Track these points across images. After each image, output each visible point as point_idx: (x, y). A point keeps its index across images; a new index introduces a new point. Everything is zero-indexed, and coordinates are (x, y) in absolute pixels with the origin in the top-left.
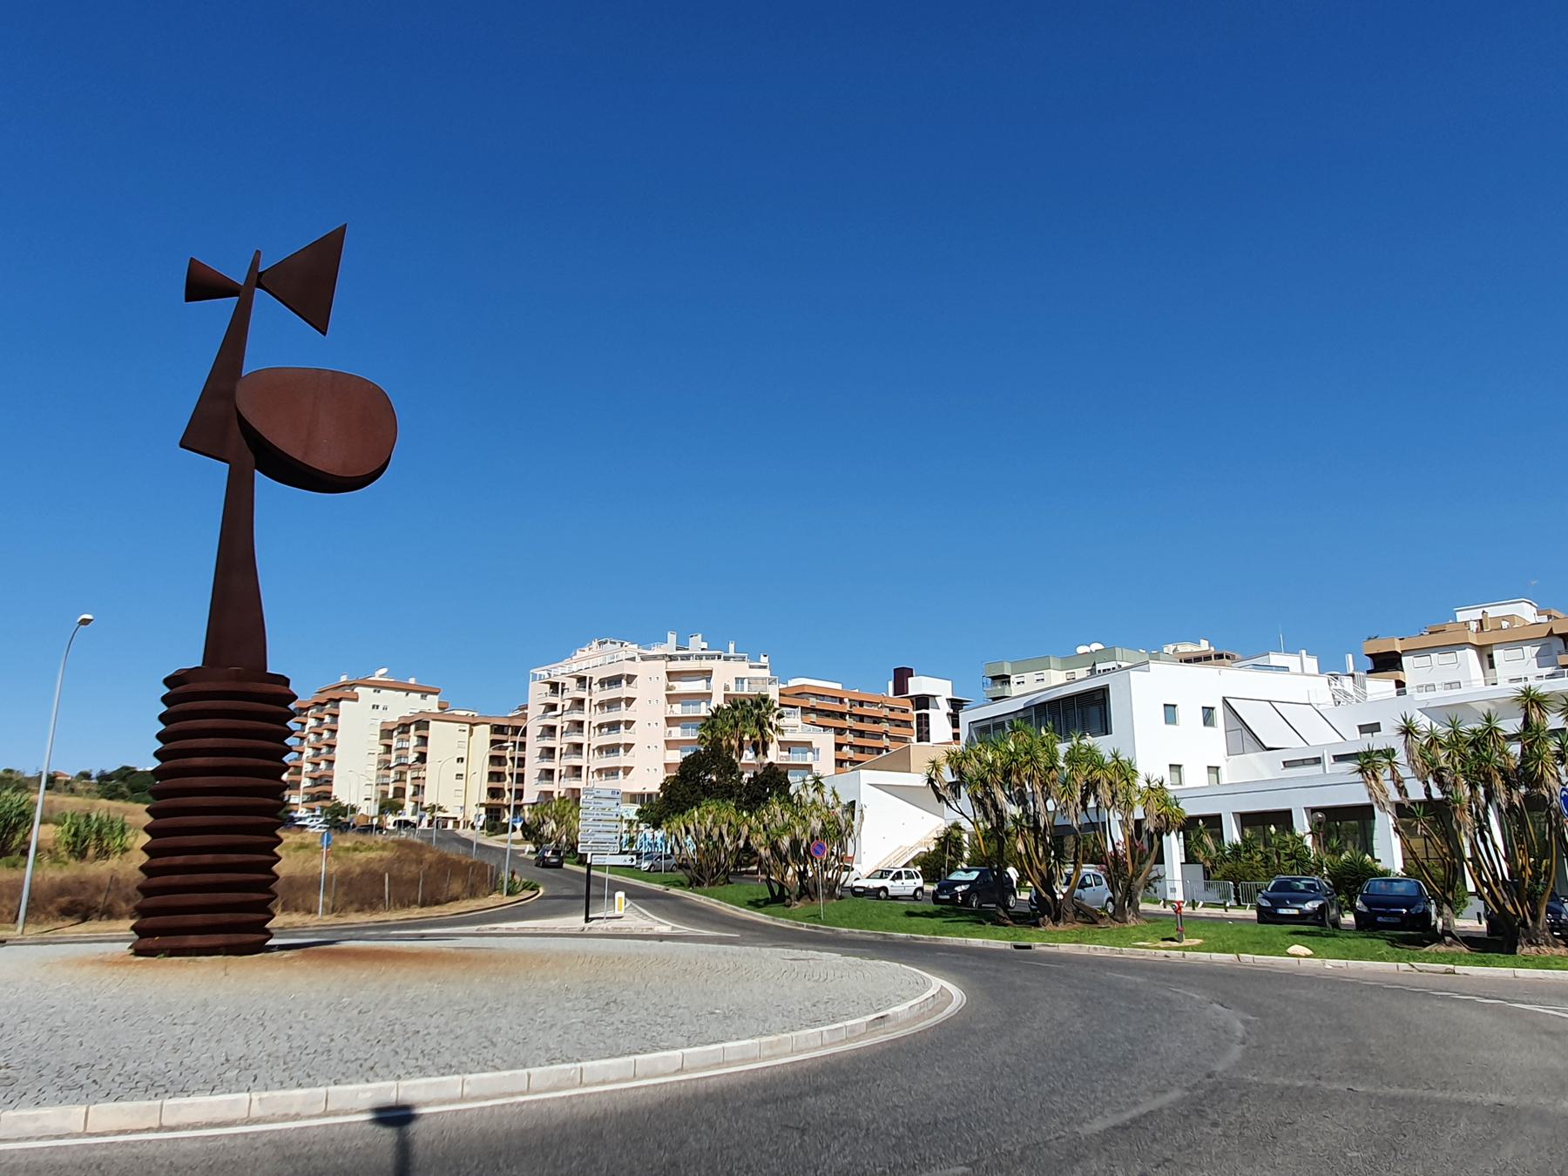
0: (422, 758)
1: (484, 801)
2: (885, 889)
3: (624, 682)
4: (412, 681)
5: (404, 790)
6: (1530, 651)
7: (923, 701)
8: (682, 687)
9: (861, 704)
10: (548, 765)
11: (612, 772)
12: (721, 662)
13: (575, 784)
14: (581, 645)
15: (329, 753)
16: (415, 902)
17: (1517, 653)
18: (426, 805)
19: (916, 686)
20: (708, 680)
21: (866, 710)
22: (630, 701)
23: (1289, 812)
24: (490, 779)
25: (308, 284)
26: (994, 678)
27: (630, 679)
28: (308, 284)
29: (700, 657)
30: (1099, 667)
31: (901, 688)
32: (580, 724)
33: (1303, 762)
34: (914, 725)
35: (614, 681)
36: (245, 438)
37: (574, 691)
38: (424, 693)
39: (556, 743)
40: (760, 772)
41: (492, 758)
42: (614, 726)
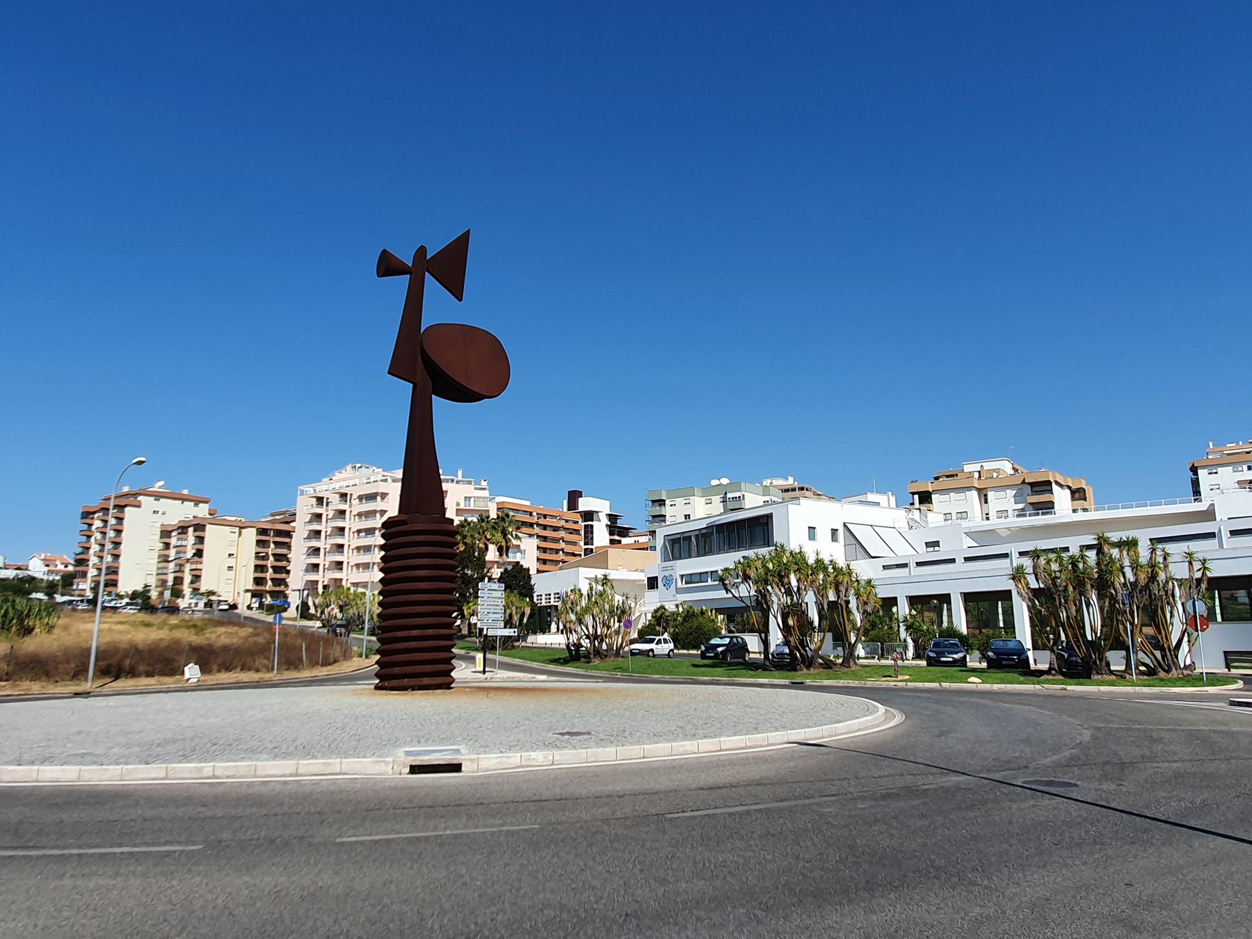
0: (199, 553)
1: (250, 587)
2: (652, 650)
3: (379, 498)
4: (185, 492)
5: (182, 579)
6: (1011, 493)
7: (589, 516)
9: (545, 516)
10: (314, 560)
12: (454, 484)
13: (338, 575)
14: (340, 467)
15: (115, 548)
16: (317, 663)
17: (1002, 494)
18: (202, 590)
19: (584, 504)
21: (548, 521)
23: (949, 595)
24: (256, 571)
25: (450, 266)
26: (654, 501)
28: (450, 266)
30: (729, 495)
31: (573, 505)
32: (342, 529)
33: (899, 566)
34: (582, 533)
35: (371, 497)
37: (336, 504)
38: (197, 502)
40: (510, 568)
41: (256, 566)
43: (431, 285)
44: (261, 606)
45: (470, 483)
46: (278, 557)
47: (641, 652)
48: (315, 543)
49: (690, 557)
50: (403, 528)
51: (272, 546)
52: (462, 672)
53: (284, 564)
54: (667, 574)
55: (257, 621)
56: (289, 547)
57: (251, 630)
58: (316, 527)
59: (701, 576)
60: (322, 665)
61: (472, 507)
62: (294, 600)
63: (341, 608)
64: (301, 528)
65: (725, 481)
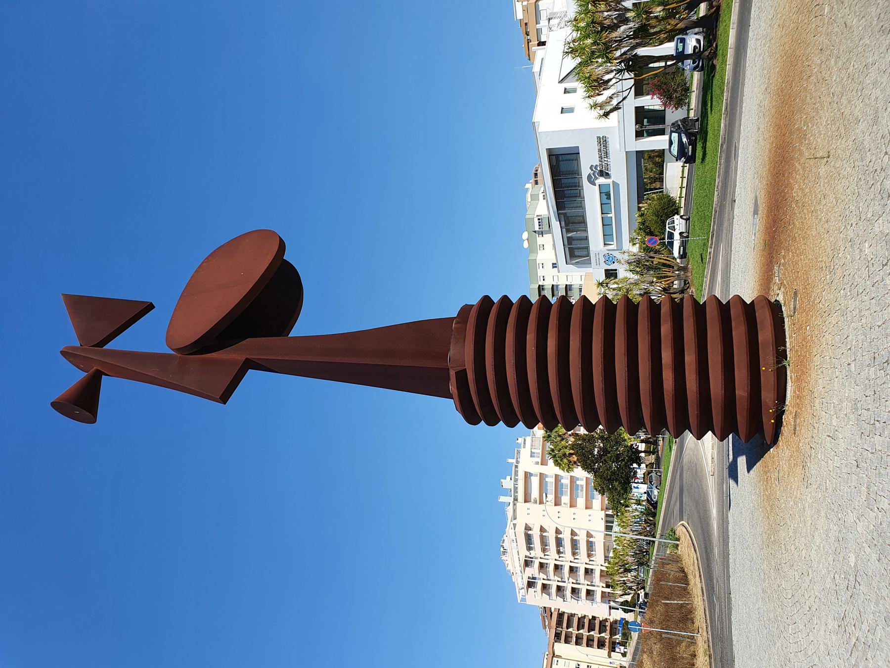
2: (681, 234)
3: (530, 532)
8: (535, 493)
11: (590, 546)
12: (520, 465)
13: (597, 574)
14: (503, 565)
16: (685, 589)
20: (531, 475)
22: (542, 529)
23: (636, 108)
24: (592, 646)
27: (528, 528)
29: (516, 480)
30: (537, 229)
35: (529, 539)
36: (258, 320)
37: (534, 571)
39: (568, 586)
41: (577, 643)
42: (559, 542)
43: (126, 342)
44: (623, 644)
45: (519, 452)
46: (580, 626)
47: (684, 245)
48: (568, 593)
49: (587, 238)
50: (470, 376)
51: (570, 630)
52: (743, 284)
53: (586, 621)
54: (602, 260)
55: (636, 649)
56: (572, 615)
57: (645, 656)
58: (554, 590)
59: (606, 224)
60: (688, 584)
61: (540, 451)
62: (618, 615)
63: (627, 570)
64: (556, 604)
65: (525, 235)
